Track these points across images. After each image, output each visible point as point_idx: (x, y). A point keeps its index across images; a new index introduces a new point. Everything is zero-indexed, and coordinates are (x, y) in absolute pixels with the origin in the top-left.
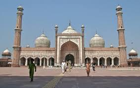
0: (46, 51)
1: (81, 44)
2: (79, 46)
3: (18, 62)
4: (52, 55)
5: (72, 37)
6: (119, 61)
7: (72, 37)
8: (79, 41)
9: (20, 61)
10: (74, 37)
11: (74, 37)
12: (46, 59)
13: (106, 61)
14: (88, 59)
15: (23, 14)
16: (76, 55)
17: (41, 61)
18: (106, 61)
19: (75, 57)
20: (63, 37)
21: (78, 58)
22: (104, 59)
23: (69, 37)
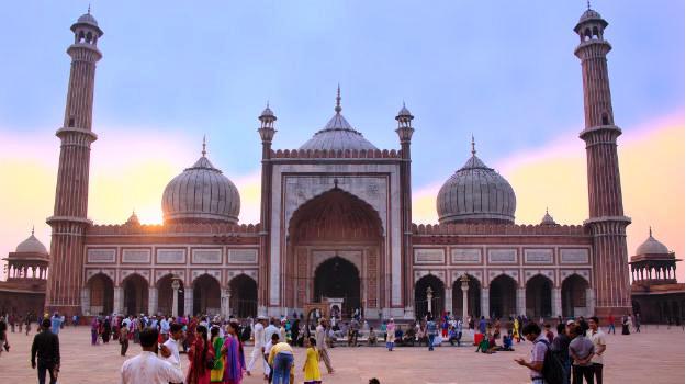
0: (216, 240)
1: (396, 205)
2: (383, 216)
3: (78, 299)
4: (239, 261)
5: (351, 168)
6: (590, 294)
7: (351, 168)
8: (383, 191)
9: (85, 294)
10: (362, 168)
11: (362, 168)
12: (474, 285)
13: (521, 295)
14: (431, 284)
15: (412, 130)
16: (372, 263)
17: (449, 295)
18: (521, 295)
19: (364, 273)
20: (298, 168)
21: (383, 277)
22: (144, 284)
23: (334, 169)
